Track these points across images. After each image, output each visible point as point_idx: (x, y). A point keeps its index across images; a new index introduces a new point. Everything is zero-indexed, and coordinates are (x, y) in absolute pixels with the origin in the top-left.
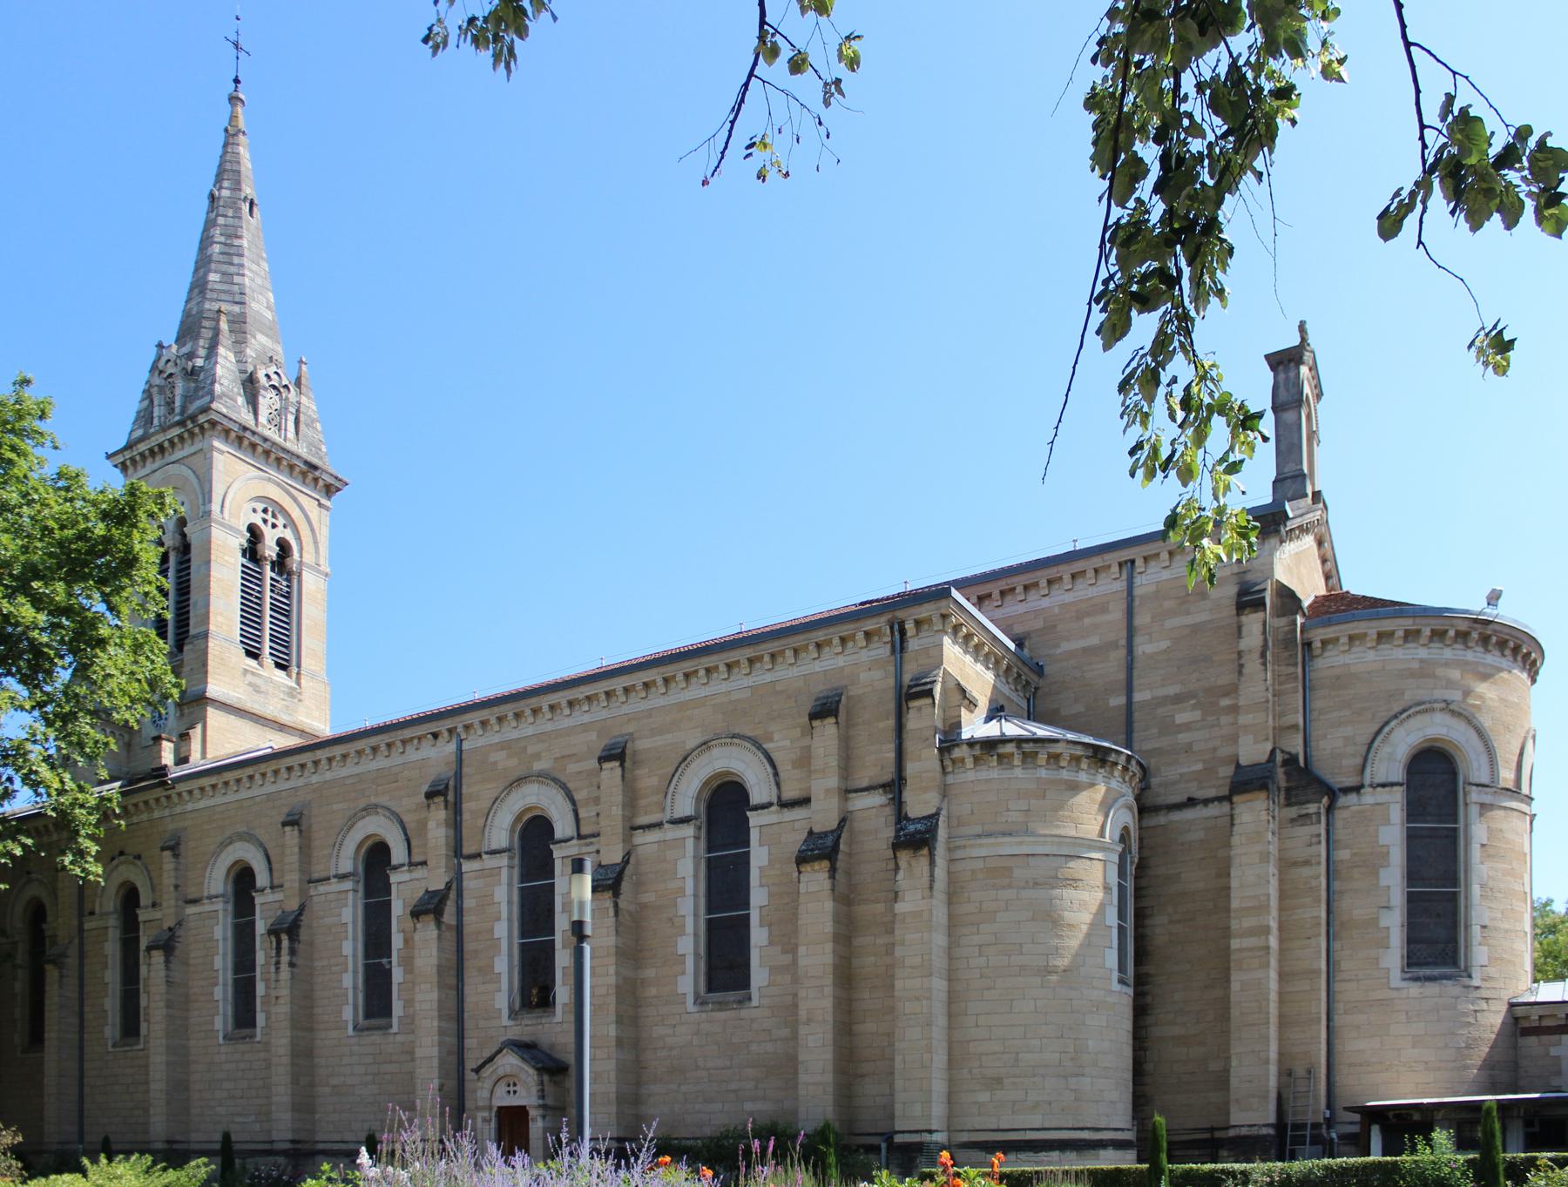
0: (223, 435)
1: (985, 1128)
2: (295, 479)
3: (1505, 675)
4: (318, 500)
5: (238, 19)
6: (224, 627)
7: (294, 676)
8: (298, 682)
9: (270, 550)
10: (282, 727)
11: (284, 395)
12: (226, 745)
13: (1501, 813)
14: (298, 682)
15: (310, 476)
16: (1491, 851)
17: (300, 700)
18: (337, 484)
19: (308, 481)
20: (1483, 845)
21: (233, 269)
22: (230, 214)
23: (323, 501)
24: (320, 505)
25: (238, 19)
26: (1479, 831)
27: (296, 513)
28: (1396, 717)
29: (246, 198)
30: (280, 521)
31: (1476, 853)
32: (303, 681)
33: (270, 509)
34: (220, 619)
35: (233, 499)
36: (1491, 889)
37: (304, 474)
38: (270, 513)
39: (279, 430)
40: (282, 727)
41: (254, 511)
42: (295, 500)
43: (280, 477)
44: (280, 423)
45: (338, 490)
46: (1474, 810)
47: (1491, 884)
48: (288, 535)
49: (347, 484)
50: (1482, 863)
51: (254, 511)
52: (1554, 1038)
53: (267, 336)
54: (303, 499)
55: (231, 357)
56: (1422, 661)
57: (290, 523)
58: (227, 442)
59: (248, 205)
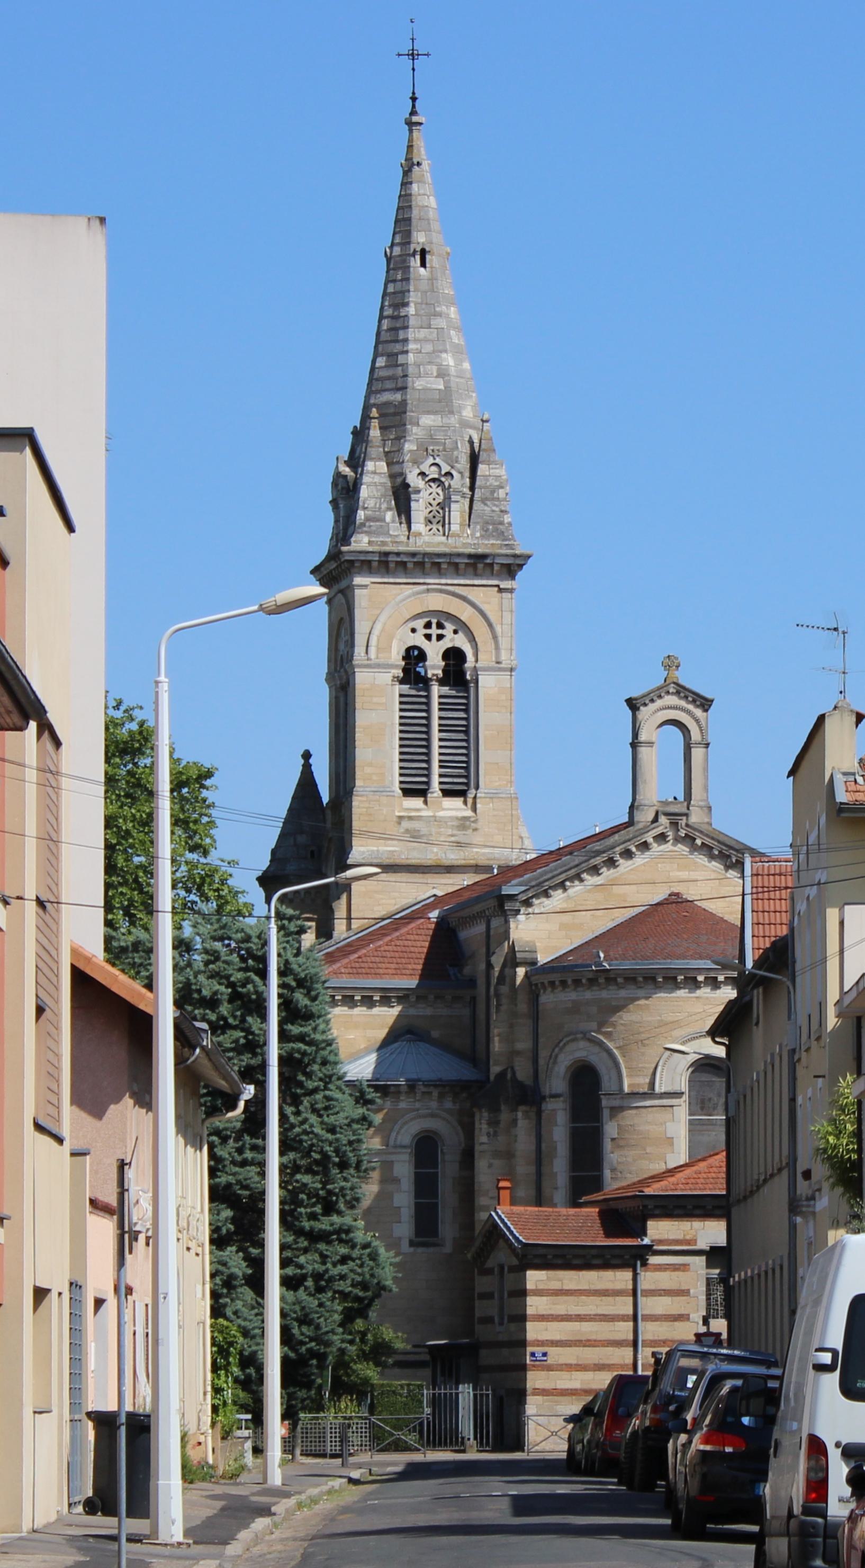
0: (365, 567)
1: (132, 1341)
2: (464, 576)
3: (642, 1002)
4: (498, 586)
5: (412, 22)
6: (375, 778)
7: (470, 801)
8: (474, 809)
9: (434, 665)
10: (450, 869)
11: (447, 484)
12: (376, 908)
13: (633, 1112)
14: (474, 809)
15: (480, 566)
16: (622, 1143)
17: (475, 830)
18: (519, 562)
19: (479, 571)
20: (613, 1139)
21: (398, 347)
22: (399, 277)
23: (504, 585)
24: (501, 590)
25: (412, 22)
26: (611, 1129)
27: (465, 613)
28: (557, 1045)
29: (415, 251)
30: (449, 627)
31: (608, 1145)
32: (478, 806)
33: (434, 621)
34: (368, 770)
35: (383, 630)
36: (621, 1172)
37: (474, 566)
38: (434, 626)
39: (443, 526)
40: (450, 869)
41: (413, 631)
42: (464, 599)
43: (443, 581)
44: (444, 517)
45: (521, 566)
46: (606, 1113)
47: (620, 1168)
48: (460, 641)
49: (529, 557)
50: (612, 1153)
51: (413, 631)
52: (541, 1287)
53: (435, 413)
54: (471, 594)
55: (382, 466)
56: (573, 1001)
57: (461, 626)
58: (371, 573)
59: (418, 257)
